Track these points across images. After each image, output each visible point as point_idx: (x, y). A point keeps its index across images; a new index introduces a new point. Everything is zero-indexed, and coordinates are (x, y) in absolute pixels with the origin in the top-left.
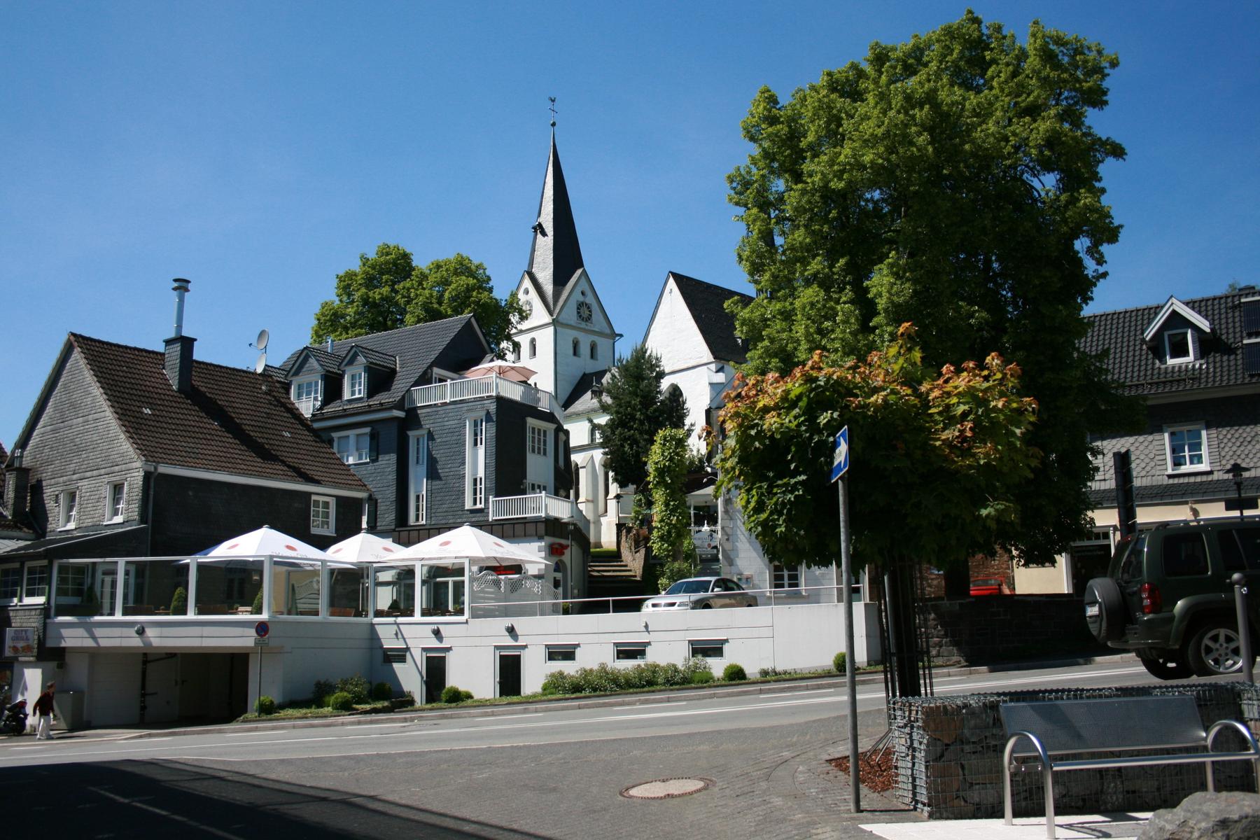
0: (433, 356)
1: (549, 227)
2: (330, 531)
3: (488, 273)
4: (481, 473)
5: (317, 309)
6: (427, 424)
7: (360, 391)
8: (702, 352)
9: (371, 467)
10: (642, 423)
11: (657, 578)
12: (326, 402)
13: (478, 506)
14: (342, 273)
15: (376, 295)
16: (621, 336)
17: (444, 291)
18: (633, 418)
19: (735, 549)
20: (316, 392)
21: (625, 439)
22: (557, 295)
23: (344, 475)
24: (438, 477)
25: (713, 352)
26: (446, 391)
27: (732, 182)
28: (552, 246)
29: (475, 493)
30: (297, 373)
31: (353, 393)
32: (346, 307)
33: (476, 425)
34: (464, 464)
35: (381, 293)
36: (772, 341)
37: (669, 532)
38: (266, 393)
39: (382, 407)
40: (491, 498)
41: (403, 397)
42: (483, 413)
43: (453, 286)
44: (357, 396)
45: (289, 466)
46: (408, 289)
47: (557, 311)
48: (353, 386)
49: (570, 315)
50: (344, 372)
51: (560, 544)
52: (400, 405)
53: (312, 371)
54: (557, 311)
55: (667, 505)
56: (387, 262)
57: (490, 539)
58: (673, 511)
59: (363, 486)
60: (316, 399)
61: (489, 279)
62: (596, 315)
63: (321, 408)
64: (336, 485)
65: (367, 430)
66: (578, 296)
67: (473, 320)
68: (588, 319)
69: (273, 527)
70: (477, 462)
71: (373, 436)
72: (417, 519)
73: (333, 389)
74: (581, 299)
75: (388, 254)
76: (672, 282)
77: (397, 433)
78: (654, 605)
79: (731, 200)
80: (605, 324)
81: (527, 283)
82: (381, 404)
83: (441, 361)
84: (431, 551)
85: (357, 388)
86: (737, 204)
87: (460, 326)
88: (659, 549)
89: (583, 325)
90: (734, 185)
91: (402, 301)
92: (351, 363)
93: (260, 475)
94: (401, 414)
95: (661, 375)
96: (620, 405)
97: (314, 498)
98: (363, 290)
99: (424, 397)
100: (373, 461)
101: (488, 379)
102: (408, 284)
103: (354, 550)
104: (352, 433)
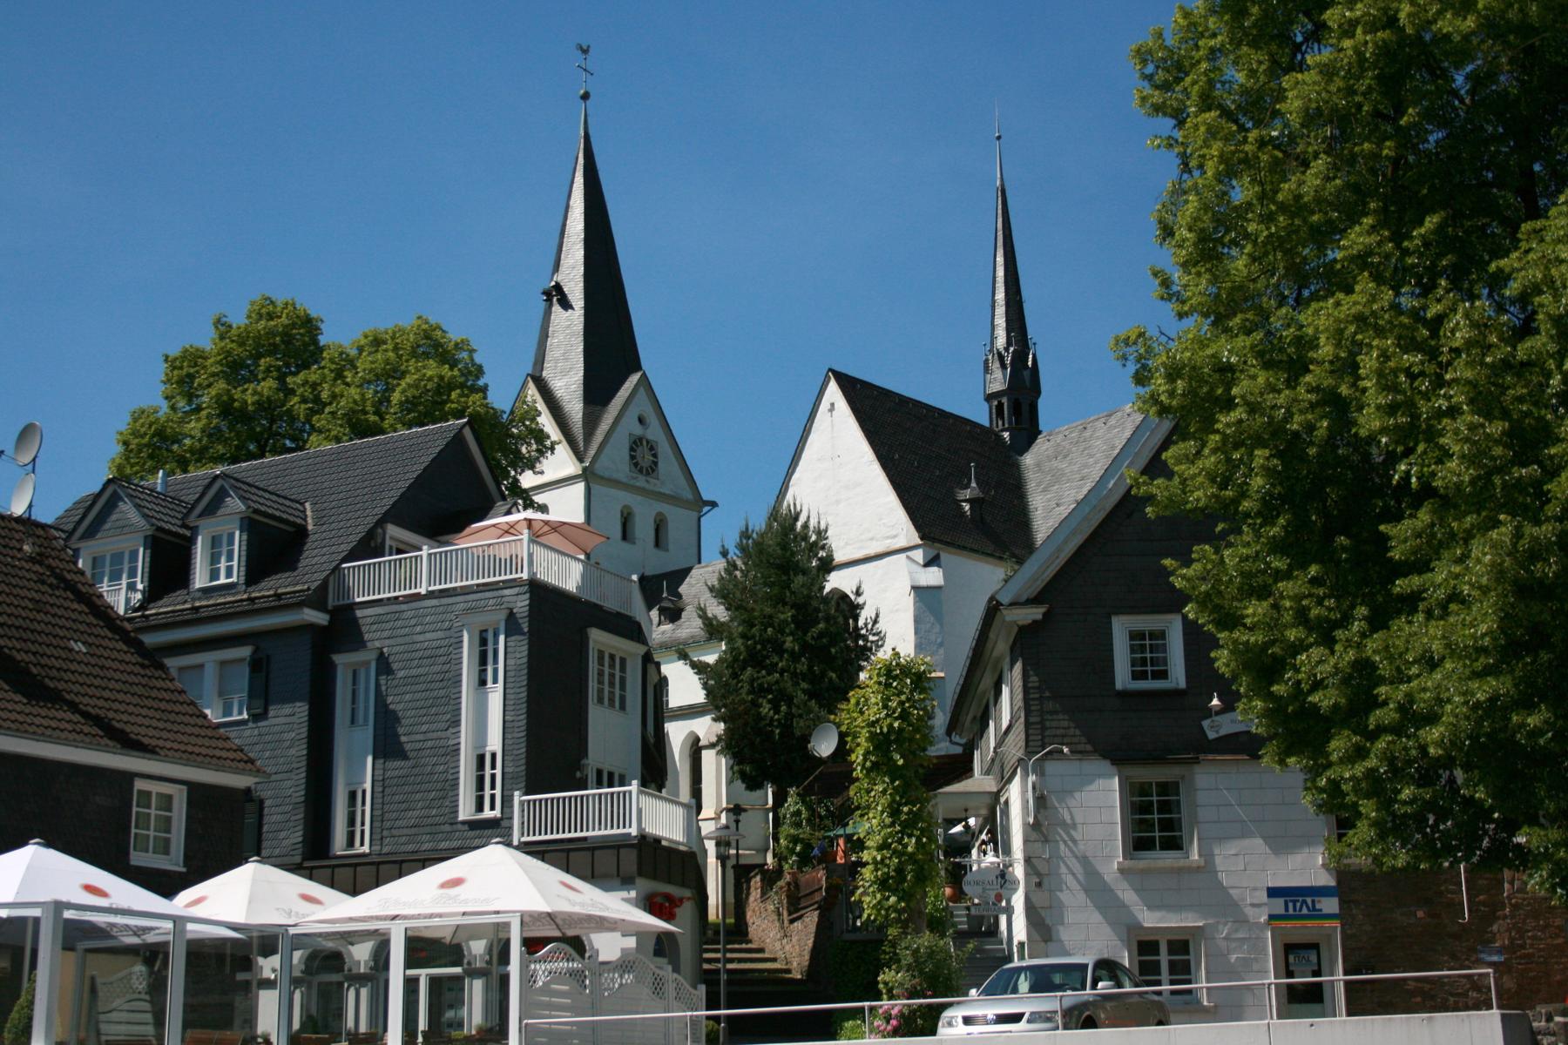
0: (387, 502)
1: (575, 290)
2: (173, 862)
3: (478, 359)
4: (494, 743)
5: (123, 423)
6: (375, 638)
7: (231, 571)
8: (897, 525)
9: (250, 732)
10: (795, 657)
11: (878, 967)
12: (152, 596)
13: (488, 813)
14: (175, 352)
15: (248, 395)
16: (714, 504)
17: (390, 389)
18: (779, 650)
19: (1059, 907)
20: (132, 574)
21: (761, 691)
22: (591, 422)
23: (211, 744)
24: (401, 754)
25: (918, 527)
26: (424, 568)
27: (1144, 62)
28: (581, 327)
29: (480, 785)
30: (91, 533)
31: (214, 575)
32: (182, 422)
33: (483, 642)
34: (457, 723)
35: (259, 389)
36: (1253, 408)
37: (900, 870)
38: (31, 559)
39: (280, 603)
40: (518, 797)
41: (325, 583)
42: (503, 615)
43: (408, 379)
44: (223, 580)
45: (86, 715)
46: (314, 386)
47: (592, 452)
48: (214, 559)
49: (617, 461)
50: (195, 531)
51: (668, 897)
52: (317, 599)
53: (124, 528)
54: (592, 452)
55: (894, 812)
56: (271, 333)
57: (552, 875)
58: (908, 827)
59: (247, 763)
60: (131, 587)
61: (480, 371)
62: (667, 464)
63: (143, 606)
64: (189, 758)
65: (245, 652)
66: (631, 426)
67: (467, 432)
68: (651, 470)
69: (50, 843)
70: (488, 718)
71: (258, 665)
72: (351, 844)
73: (170, 566)
74: (638, 430)
75: (271, 317)
76: (833, 392)
77: (310, 656)
78: (968, 1021)
79: (1144, 99)
80: (682, 482)
81: (532, 392)
82: (278, 596)
83: (396, 515)
84: (415, 899)
85: (223, 565)
86: (1158, 109)
87: (440, 445)
88: (878, 906)
89: (641, 481)
90: (1150, 69)
91: (301, 410)
92: (212, 509)
93: (20, 731)
94: (320, 618)
95: (828, 566)
96: (750, 624)
97: (139, 785)
98: (221, 385)
99: (371, 584)
100: (255, 718)
101: (499, 547)
102: (313, 375)
103: (234, 899)
104: (210, 659)
